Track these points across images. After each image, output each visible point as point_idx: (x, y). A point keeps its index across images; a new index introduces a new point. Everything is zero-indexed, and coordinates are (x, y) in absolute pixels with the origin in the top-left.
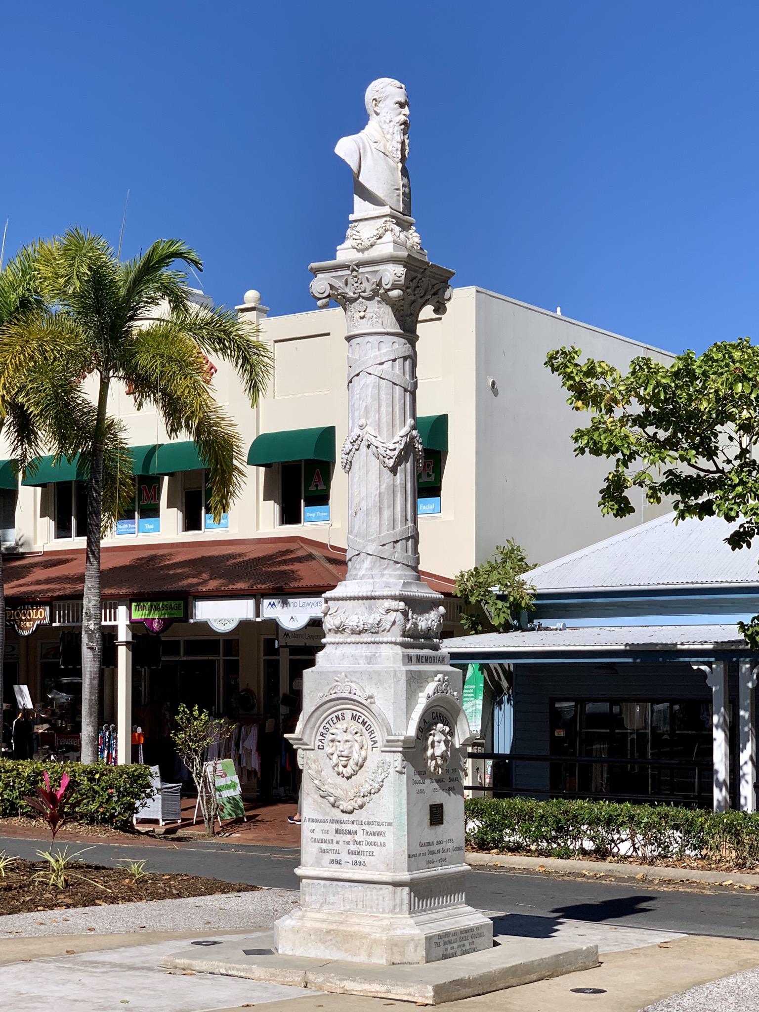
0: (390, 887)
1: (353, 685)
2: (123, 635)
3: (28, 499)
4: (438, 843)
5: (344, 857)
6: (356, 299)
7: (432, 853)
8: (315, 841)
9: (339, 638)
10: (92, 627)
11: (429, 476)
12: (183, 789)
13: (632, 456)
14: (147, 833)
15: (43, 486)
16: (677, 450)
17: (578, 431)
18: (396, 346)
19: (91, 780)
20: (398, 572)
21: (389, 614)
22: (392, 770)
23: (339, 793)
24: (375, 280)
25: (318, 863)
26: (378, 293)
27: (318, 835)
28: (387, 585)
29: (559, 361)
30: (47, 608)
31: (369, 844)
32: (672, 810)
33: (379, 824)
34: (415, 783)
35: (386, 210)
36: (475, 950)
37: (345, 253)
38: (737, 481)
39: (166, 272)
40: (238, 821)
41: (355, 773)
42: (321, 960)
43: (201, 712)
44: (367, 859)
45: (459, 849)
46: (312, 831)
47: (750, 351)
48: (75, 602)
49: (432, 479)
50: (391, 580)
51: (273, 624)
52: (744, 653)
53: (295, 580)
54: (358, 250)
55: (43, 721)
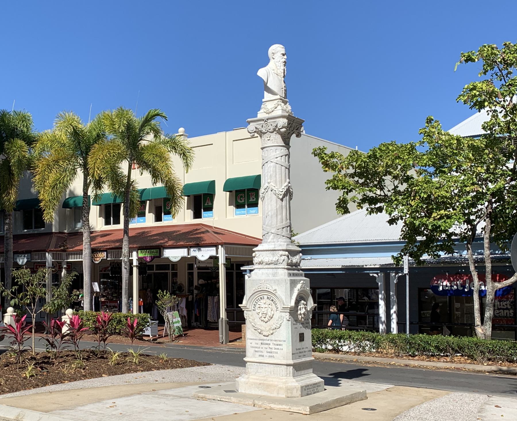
0: (285, 366)
1: (268, 285)
2: (135, 263)
3: (94, 210)
4: (303, 348)
5: (265, 354)
6: (266, 133)
7: (300, 353)
8: (252, 347)
9: (260, 266)
10: (126, 260)
11: (253, 199)
12: (158, 323)
13: (351, 191)
14: (148, 341)
15: (100, 205)
16: (368, 187)
17: (328, 180)
18: (282, 151)
19: (126, 320)
20: (284, 240)
21: (282, 258)
22: (285, 319)
23: (262, 328)
24: (275, 125)
25: (254, 356)
26: (276, 130)
27: (254, 345)
28: (280, 245)
29: (319, 153)
30: (105, 253)
31: (275, 349)
32: (366, 334)
33: (279, 341)
34: (294, 324)
35: (278, 97)
36: (318, 392)
37: (261, 115)
38: (394, 199)
39: (153, 122)
40: (180, 336)
41: (269, 320)
42: (258, 395)
43: (167, 293)
44: (275, 355)
45: (310, 351)
46: (251, 343)
47: (396, 146)
48: (120, 250)
49: (255, 200)
50: (281, 243)
51: (195, 258)
52: (393, 269)
53: (203, 241)
54: (267, 113)
55: (103, 296)
